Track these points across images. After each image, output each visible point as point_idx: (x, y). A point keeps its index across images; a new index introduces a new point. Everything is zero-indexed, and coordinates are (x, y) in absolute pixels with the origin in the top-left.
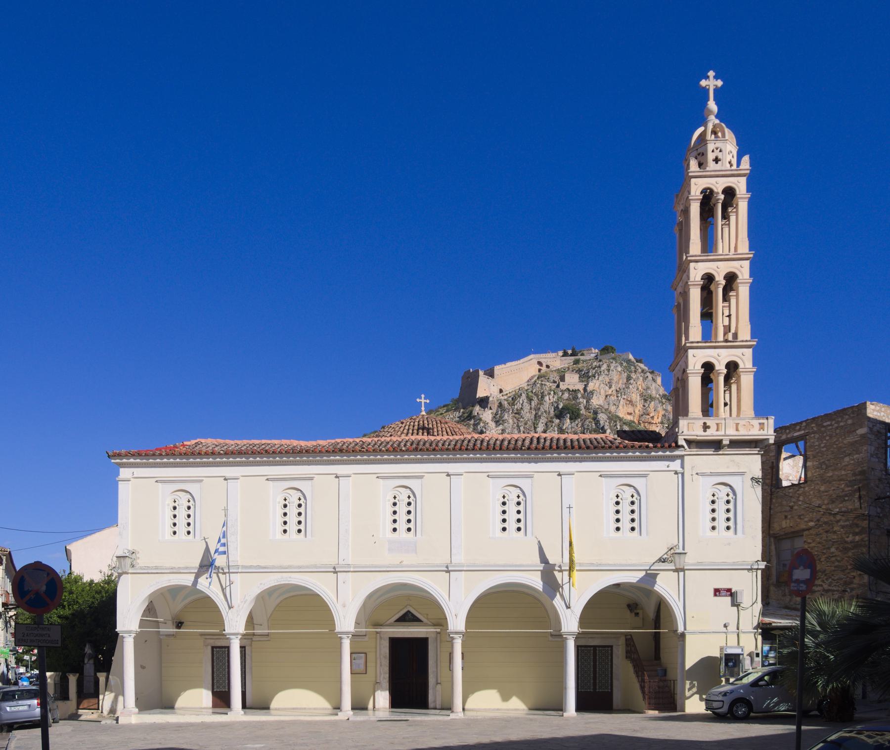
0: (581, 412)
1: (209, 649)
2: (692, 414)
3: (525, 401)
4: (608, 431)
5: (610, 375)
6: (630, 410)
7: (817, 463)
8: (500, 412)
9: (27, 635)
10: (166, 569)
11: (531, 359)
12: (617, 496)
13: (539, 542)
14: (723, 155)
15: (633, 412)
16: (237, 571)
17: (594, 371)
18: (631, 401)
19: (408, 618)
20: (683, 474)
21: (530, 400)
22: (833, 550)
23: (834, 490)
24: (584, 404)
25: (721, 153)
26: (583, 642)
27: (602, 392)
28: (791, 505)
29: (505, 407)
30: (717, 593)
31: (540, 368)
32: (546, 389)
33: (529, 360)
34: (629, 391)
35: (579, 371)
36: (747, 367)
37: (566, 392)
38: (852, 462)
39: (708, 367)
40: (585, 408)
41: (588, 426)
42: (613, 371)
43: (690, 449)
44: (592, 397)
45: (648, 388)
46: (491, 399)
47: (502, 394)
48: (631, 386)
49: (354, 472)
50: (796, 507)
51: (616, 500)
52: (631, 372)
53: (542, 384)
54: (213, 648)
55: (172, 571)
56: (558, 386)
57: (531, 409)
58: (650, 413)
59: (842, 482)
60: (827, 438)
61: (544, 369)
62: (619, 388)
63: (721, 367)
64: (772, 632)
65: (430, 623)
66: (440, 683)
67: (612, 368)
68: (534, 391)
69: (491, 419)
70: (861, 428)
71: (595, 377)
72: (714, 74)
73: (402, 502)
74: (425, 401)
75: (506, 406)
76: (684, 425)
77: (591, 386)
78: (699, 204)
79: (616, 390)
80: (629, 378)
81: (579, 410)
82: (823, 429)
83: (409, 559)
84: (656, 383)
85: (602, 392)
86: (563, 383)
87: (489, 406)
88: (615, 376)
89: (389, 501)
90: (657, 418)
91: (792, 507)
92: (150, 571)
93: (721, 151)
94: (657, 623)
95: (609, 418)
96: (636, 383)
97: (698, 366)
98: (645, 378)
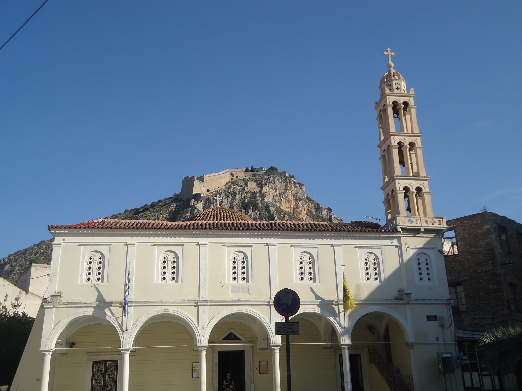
0: (259, 205)
1: (91, 363)
2: (402, 214)
3: (224, 197)
4: (276, 218)
5: (275, 184)
6: (288, 205)
7: (464, 243)
8: (208, 204)
9: (282, 329)
10: (82, 304)
11: (227, 172)
12: (426, 260)
13: (311, 288)
14: (400, 86)
15: (289, 207)
16: (132, 305)
17: (265, 181)
18: (288, 200)
19: (231, 337)
20: (401, 247)
21: (227, 197)
22: (482, 293)
23: (476, 259)
24: (260, 201)
25: (399, 85)
26: (352, 352)
27: (271, 194)
28: (452, 266)
29: (211, 200)
30: (429, 319)
31: (232, 177)
32: (237, 191)
33: (226, 173)
34: (287, 194)
35: (256, 181)
36: (427, 190)
37: (249, 193)
38: (484, 243)
39: (406, 189)
40: (261, 203)
41: (263, 214)
42: (277, 182)
43: (403, 233)
44: (265, 197)
45: (297, 193)
46: (202, 195)
47: (208, 192)
48: (288, 191)
49: (138, 242)
50: (455, 268)
51: (366, 261)
52: (287, 183)
53: (234, 187)
54: (94, 362)
55: (85, 305)
56: (244, 189)
57: (227, 202)
58: (300, 208)
59: (481, 254)
60: (468, 230)
61: (235, 178)
62: (281, 192)
63: (413, 189)
64: (463, 343)
65: (246, 341)
66: (253, 383)
67: (276, 180)
68: (229, 191)
69: (202, 208)
70: (486, 225)
71: (266, 185)
72: (390, 49)
73: (169, 261)
74: (217, 198)
75: (212, 200)
76: (399, 220)
77: (264, 190)
78: (392, 108)
79: (279, 193)
80: (286, 186)
81: (258, 204)
82: (464, 225)
83: (245, 297)
84: (302, 190)
85: (271, 194)
86: (247, 187)
87: (201, 200)
88: (278, 185)
89: (298, 261)
90: (304, 210)
91: (453, 268)
92: (70, 306)
93: (399, 85)
94: (387, 337)
95: (276, 210)
96: (291, 190)
97: (402, 189)
98: (296, 187)
